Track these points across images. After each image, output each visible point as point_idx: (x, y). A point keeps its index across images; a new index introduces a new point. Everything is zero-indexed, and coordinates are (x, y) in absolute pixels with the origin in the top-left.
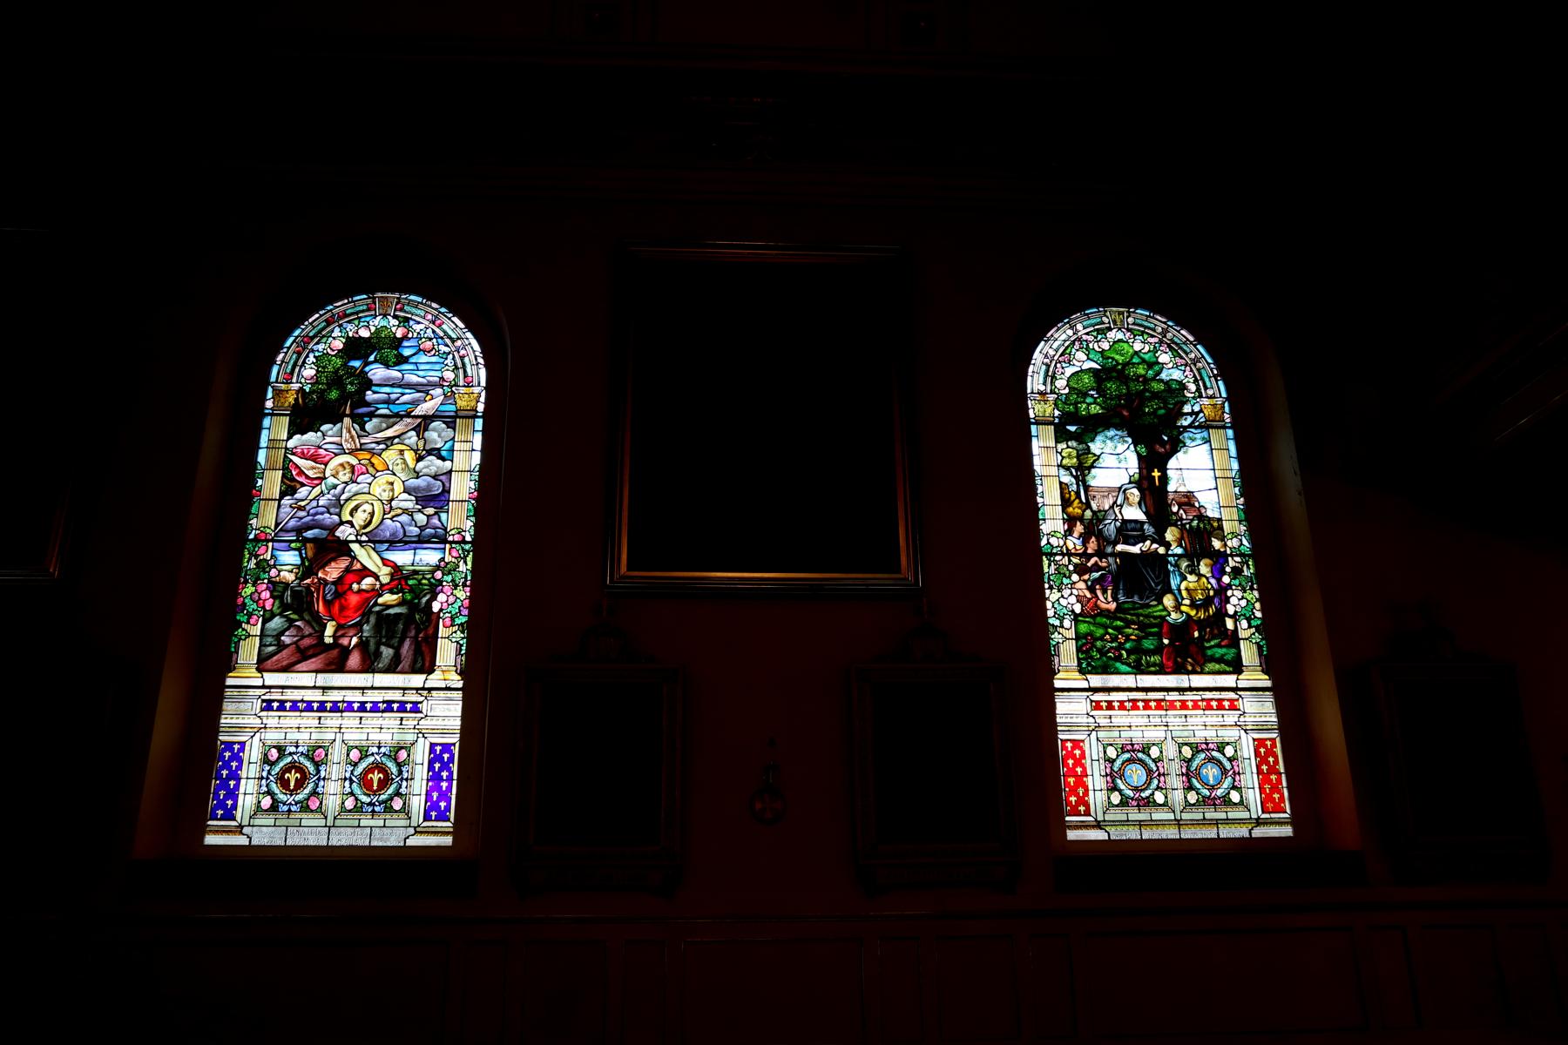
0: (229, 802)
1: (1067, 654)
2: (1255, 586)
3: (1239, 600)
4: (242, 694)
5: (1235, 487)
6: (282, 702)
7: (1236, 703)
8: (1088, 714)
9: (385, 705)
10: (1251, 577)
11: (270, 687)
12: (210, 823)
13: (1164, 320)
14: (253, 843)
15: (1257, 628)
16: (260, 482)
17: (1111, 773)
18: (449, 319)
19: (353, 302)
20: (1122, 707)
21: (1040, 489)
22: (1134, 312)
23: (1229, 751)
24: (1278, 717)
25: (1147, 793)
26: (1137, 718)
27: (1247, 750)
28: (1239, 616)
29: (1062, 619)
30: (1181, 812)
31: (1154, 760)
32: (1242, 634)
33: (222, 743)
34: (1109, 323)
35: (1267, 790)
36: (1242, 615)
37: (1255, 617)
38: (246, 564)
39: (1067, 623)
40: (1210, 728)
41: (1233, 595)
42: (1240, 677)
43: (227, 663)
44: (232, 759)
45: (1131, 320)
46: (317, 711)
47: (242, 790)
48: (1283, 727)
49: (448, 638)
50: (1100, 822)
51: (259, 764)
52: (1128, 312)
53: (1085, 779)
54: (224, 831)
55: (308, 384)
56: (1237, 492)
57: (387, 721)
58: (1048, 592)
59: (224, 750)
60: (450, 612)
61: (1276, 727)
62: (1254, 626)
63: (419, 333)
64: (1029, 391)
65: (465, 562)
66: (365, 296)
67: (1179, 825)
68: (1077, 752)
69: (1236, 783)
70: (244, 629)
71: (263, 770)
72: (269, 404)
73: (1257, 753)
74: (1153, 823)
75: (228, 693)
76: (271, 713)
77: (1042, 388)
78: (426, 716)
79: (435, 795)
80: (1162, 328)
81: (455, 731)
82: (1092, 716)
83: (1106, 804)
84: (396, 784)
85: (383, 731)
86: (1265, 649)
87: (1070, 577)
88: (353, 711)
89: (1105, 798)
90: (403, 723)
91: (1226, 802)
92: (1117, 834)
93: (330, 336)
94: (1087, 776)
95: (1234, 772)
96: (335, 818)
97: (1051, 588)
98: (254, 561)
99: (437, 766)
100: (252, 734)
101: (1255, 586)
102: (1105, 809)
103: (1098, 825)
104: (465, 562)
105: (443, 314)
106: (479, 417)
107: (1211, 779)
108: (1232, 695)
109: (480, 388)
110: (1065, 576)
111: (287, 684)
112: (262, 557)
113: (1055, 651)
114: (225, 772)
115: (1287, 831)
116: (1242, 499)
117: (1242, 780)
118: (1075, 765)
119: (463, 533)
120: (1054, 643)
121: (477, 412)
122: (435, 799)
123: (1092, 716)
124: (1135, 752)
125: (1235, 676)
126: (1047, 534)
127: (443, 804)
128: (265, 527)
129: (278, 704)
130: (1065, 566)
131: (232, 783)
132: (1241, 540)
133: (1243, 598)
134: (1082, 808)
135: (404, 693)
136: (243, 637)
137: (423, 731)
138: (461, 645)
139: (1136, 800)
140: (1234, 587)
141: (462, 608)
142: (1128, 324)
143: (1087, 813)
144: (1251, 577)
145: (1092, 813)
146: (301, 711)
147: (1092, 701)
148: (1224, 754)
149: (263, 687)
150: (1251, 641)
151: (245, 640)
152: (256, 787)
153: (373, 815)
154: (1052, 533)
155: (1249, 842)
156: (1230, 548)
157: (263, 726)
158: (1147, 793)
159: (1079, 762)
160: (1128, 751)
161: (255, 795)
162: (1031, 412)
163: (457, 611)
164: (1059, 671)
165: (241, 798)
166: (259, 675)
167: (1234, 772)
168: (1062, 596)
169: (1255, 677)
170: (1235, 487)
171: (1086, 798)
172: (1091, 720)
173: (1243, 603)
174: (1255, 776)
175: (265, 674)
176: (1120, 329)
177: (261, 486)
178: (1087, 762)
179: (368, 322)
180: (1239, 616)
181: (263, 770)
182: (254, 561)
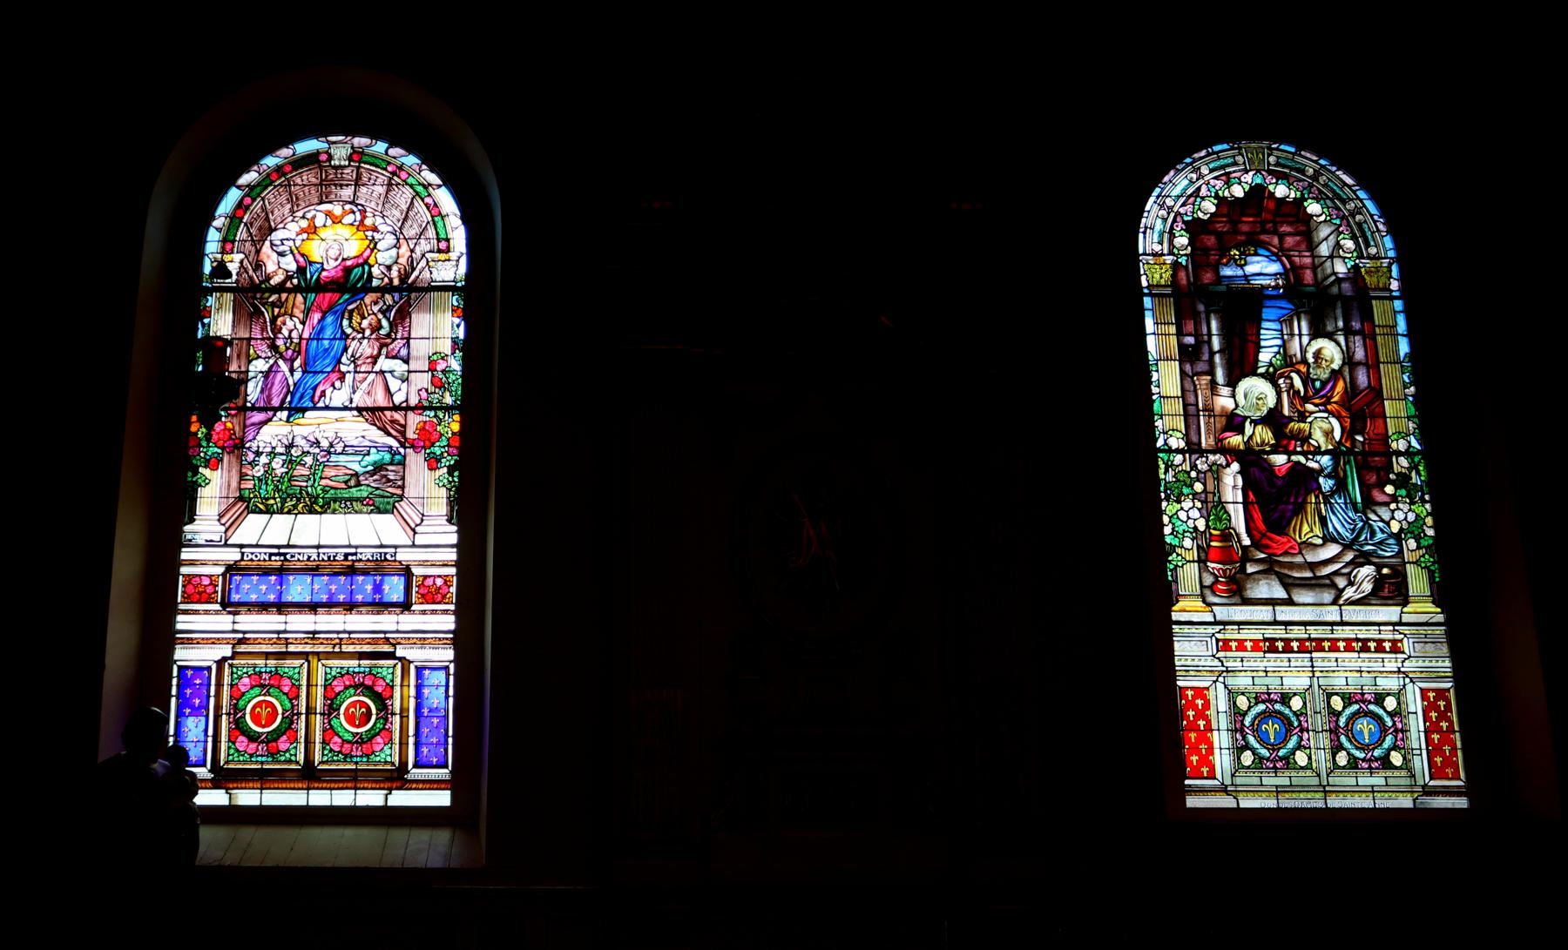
1: (1189, 576)
2: (1427, 497)
5: (1403, 373)
6: (1287, 641)
7: (1399, 644)
8: (1213, 656)
10: (1421, 486)
13: (1315, 158)
15: (1427, 548)
19: (1214, 153)
20: (1256, 648)
21: (1155, 376)
22: (1277, 149)
23: (1390, 703)
24: (1453, 661)
27: (1415, 704)
31: (1295, 713)
34: (1244, 163)
35: (1204, 751)
37: (1425, 535)
40: (1367, 675)
42: (1405, 610)
45: (1272, 159)
48: (1458, 674)
50: (1226, 786)
52: (1270, 149)
53: (1209, 735)
55: (1182, 255)
58: (1164, 504)
61: (1450, 674)
62: (1424, 547)
64: (1141, 251)
66: (1225, 146)
67: (1325, 792)
68: (1199, 702)
69: (1303, 743)
74: (1291, 789)
76: (1229, 654)
77: (1157, 248)
78: (1410, 657)
82: (1218, 658)
84: (1390, 736)
86: (1437, 575)
87: (1191, 486)
90: (1292, 664)
93: (1198, 196)
94: (1212, 730)
97: (1168, 499)
99: (1434, 715)
101: (1427, 497)
103: (1224, 790)
104: (1418, 473)
110: (1186, 485)
111: (1317, 619)
113: (1172, 576)
115: (1461, 803)
116: (1412, 389)
117: (1311, 738)
118: (1197, 717)
120: (1172, 567)
123: (1218, 658)
124: (1274, 704)
125: (1399, 608)
130: (1185, 471)
132: (1409, 442)
134: (1205, 770)
139: (1272, 761)
140: (1400, 499)
141: (1425, 527)
142: (1269, 164)
143: (1212, 776)
145: (1218, 775)
147: (1218, 640)
148: (1384, 709)
149: (1216, 623)
153: (1276, 773)
159: (1201, 714)
160: (1263, 702)
162: (1143, 278)
164: (1178, 601)
168: (1182, 509)
169: (1423, 609)
171: (1211, 758)
172: (1217, 663)
176: (1258, 171)
178: (1211, 713)
179: (1239, 179)
180: (1405, 535)
182: (1171, 473)
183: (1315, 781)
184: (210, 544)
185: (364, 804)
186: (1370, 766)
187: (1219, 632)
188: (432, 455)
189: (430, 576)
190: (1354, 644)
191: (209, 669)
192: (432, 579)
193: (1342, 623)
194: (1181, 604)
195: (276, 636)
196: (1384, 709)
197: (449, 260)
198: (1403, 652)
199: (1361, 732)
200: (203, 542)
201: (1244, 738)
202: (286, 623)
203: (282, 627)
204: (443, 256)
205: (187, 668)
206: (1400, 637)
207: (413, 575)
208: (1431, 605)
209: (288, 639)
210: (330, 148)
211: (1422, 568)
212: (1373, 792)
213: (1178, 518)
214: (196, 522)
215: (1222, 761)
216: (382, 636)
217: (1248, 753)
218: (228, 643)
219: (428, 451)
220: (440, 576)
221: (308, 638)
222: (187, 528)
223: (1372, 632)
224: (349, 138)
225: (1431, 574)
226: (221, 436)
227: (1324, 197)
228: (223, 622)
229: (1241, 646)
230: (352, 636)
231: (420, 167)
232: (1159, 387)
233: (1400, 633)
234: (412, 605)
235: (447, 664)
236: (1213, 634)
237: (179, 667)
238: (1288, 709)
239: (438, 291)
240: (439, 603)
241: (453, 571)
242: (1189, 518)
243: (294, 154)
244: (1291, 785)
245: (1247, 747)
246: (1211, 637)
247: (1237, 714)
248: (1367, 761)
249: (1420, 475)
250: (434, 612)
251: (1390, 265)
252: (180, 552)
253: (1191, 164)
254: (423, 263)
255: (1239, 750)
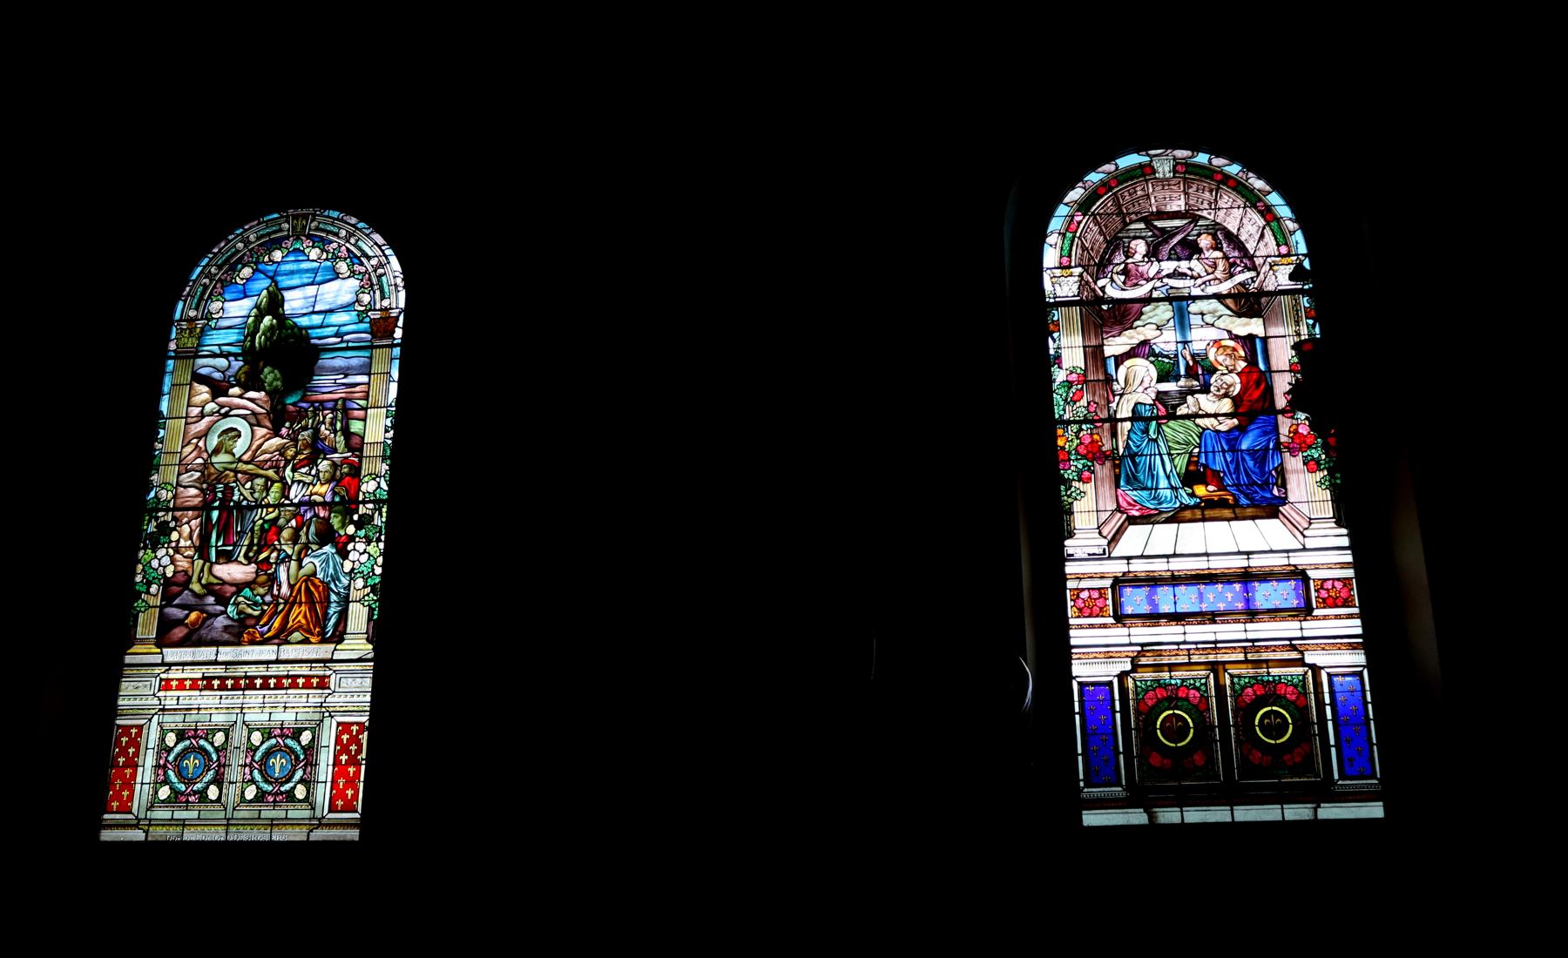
0: (125, 793)
3: (361, 554)
4: (142, 672)
5: (387, 417)
6: (266, 678)
8: (154, 695)
9: (290, 681)
10: (381, 527)
11: (170, 665)
12: (106, 816)
14: (149, 839)
15: (373, 588)
16: (162, 433)
17: (251, 763)
18: (367, 235)
19: (264, 222)
20: (194, 686)
25: (287, 787)
26: (208, 699)
27: (329, 736)
28: (356, 574)
29: (149, 584)
30: (147, 810)
32: (354, 595)
33: (119, 726)
36: (359, 572)
38: (145, 527)
39: (154, 589)
41: (354, 549)
43: (129, 640)
44: (129, 745)
45: (314, 224)
46: (303, 688)
47: (139, 779)
49: (150, 607)
51: (156, 750)
54: (345, 824)
56: (390, 425)
57: (205, 700)
59: (122, 735)
60: (363, 572)
62: (370, 586)
63: (333, 253)
65: (380, 514)
70: (143, 601)
71: (161, 757)
72: (172, 346)
73: (338, 741)
75: (127, 672)
76: (169, 693)
79: (341, 782)
80: (241, 242)
81: (365, 709)
83: (238, 799)
85: (291, 708)
88: (255, 689)
89: (238, 792)
91: (290, 796)
92: (158, 833)
95: (219, 764)
96: (234, 809)
98: (154, 523)
100: (150, 716)
101: (383, 538)
102: (149, 805)
104: (380, 514)
105: (360, 230)
106: (397, 345)
107: (277, 771)
108: (319, 671)
109: (397, 311)
111: (236, 659)
112: (162, 519)
114: (121, 760)
119: (378, 479)
121: (395, 339)
122: (341, 787)
125: (333, 646)
126: (157, 486)
127: (350, 792)
128: (166, 484)
129: (304, 680)
131: (128, 771)
132: (379, 483)
133: (365, 552)
135: (268, 668)
136: (143, 609)
137: (331, 709)
138: (374, 609)
144: (381, 527)
146: (287, 688)
147: (161, 680)
148: (212, 744)
149: (163, 664)
150: (363, 604)
151: (144, 612)
152: (153, 776)
154: (163, 485)
155: (307, 845)
156: (364, 493)
157: (162, 707)
158: (287, 787)
161: (152, 785)
163: (370, 570)
165: (138, 787)
166: (159, 650)
167: (219, 764)
170: (387, 417)
173: (364, 558)
174: (330, 768)
175: (165, 650)
177: (163, 437)
181: (161, 757)
183: (222, 815)
184: (1092, 557)
185: (1325, 817)
186: (275, 800)
187: (164, 672)
188: (1309, 458)
189: (1329, 579)
190: (284, 681)
191: (1110, 683)
192: (1331, 582)
193: (277, 662)
194: (136, 649)
195: (1176, 647)
196: (212, 744)
197: (1071, 276)
198: (329, 688)
199: (187, 767)
200: (1087, 556)
201: (165, 773)
202: (1246, 631)
203: (1180, 638)
204: (1065, 272)
205: (1088, 684)
206: (328, 673)
207: (1309, 578)
208: (153, 646)
209: (1190, 649)
210: (1151, 161)
211: (364, 606)
212: (272, 825)
213: (151, 566)
214: (346, 642)
215: (141, 794)
216: (1288, 643)
217: (166, 788)
218: (1127, 657)
219: (1305, 454)
220: (1338, 579)
221: (1211, 648)
222: (1067, 543)
223: (303, 669)
224: (1169, 151)
225: (371, 610)
226: (1089, 449)
227: (351, 256)
228: (1118, 635)
229: (181, 685)
230: (1256, 644)
231: (1247, 174)
232: (162, 443)
233: (330, 669)
234: (1313, 609)
235: (1360, 669)
236: (159, 674)
237: (1079, 683)
238: (296, 744)
239: (1065, 307)
240: (1097, 616)
241: (1350, 573)
242: (160, 565)
243: (1117, 169)
244: (286, 818)
245: (166, 782)
246: (156, 677)
247: (163, 749)
248: (272, 795)
249: (382, 517)
250: (1092, 626)
251: (400, 313)
252: (1064, 566)
253: (241, 234)
254: (1267, 267)
255: (157, 785)
